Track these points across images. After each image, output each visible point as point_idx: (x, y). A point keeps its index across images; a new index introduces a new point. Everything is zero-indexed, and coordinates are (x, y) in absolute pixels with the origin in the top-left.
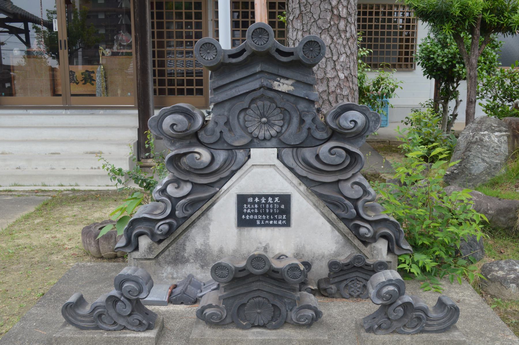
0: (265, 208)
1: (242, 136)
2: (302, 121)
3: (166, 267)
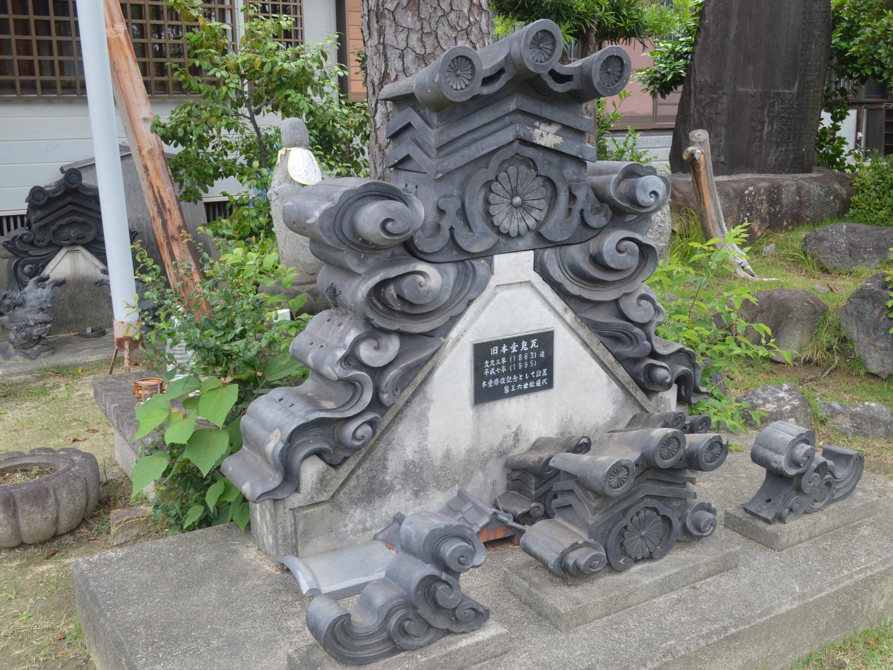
0: (517, 362)
1: (484, 234)
2: (572, 197)
3: (352, 512)
